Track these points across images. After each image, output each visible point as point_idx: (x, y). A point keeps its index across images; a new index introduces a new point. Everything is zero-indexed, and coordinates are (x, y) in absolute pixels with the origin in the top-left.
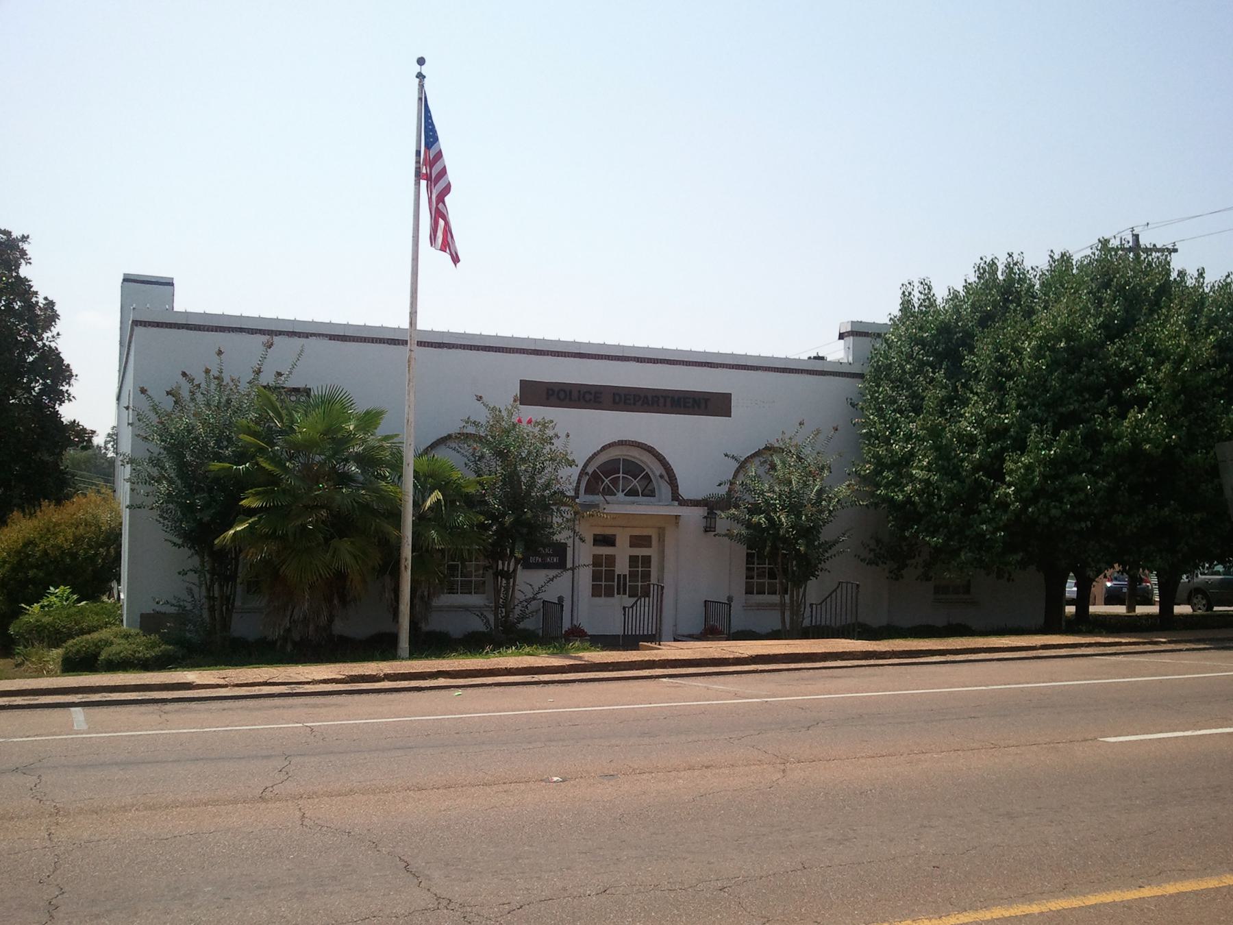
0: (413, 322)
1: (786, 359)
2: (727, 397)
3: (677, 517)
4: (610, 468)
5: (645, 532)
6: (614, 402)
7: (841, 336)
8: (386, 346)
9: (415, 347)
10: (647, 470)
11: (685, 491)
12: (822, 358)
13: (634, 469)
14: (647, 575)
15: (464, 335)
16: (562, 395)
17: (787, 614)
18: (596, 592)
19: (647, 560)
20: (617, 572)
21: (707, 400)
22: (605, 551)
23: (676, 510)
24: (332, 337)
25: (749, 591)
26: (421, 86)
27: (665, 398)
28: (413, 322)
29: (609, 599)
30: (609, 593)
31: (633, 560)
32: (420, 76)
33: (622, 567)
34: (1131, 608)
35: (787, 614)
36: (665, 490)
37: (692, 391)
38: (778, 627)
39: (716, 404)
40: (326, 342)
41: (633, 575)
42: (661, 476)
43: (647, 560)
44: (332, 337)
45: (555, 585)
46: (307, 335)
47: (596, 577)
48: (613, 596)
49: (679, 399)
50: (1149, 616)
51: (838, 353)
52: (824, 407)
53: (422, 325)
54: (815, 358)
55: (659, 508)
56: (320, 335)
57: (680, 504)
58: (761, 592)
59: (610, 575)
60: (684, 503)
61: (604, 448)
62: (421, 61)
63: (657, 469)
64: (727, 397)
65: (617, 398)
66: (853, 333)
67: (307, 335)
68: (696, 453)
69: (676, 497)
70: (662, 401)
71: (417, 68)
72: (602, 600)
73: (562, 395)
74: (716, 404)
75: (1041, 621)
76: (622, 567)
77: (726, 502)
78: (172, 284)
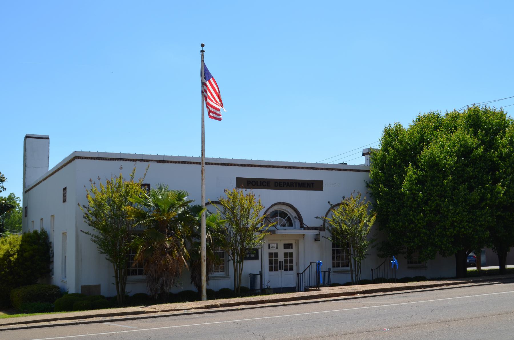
0: (203, 155)
1: (143, 155)
2: (321, 182)
3: (304, 235)
4: (274, 214)
5: (290, 242)
6: (275, 186)
7: (364, 155)
8: (181, 164)
9: (204, 165)
10: (289, 215)
11: (307, 222)
12: (346, 164)
13: (283, 214)
14: (291, 261)
15: (213, 159)
16: (254, 183)
17: (354, 275)
18: (271, 269)
19: (291, 254)
20: (279, 260)
21: (313, 184)
22: (288, 251)
23: (302, 231)
24: (159, 161)
25: (334, 267)
26: (202, 56)
27: (296, 183)
28: (203, 155)
29: (276, 272)
30: (276, 270)
31: (285, 254)
32: (202, 51)
33: (281, 258)
34: (479, 268)
35: (354, 275)
36: (297, 223)
37: (306, 181)
38: (350, 281)
39: (315, 185)
40: (156, 163)
41: (286, 261)
42: (295, 217)
43: (291, 254)
44: (159, 161)
45: (250, 267)
46: (148, 161)
47: (270, 262)
48: (277, 270)
49: (302, 183)
50: (472, 272)
51: (361, 161)
52: (357, 184)
53: (208, 155)
54: (342, 164)
55: (296, 231)
56: (153, 161)
57: (304, 229)
58: (338, 266)
59: (276, 261)
60: (305, 229)
61: (272, 206)
62: (203, 45)
63: (294, 214)
64: (321, 182)
65: (276, 184)
66: (368, 154)
67: (148, 161)
68: (309, 205)
69: (302, 226)
70: (294, 185)
71: (201, 48)
72: (273, 273)
73: (254, 183)
74: (315, 185)
75: (454, 274)
76: (281, 258)
77: (322, 229)
78: (48, 138)
